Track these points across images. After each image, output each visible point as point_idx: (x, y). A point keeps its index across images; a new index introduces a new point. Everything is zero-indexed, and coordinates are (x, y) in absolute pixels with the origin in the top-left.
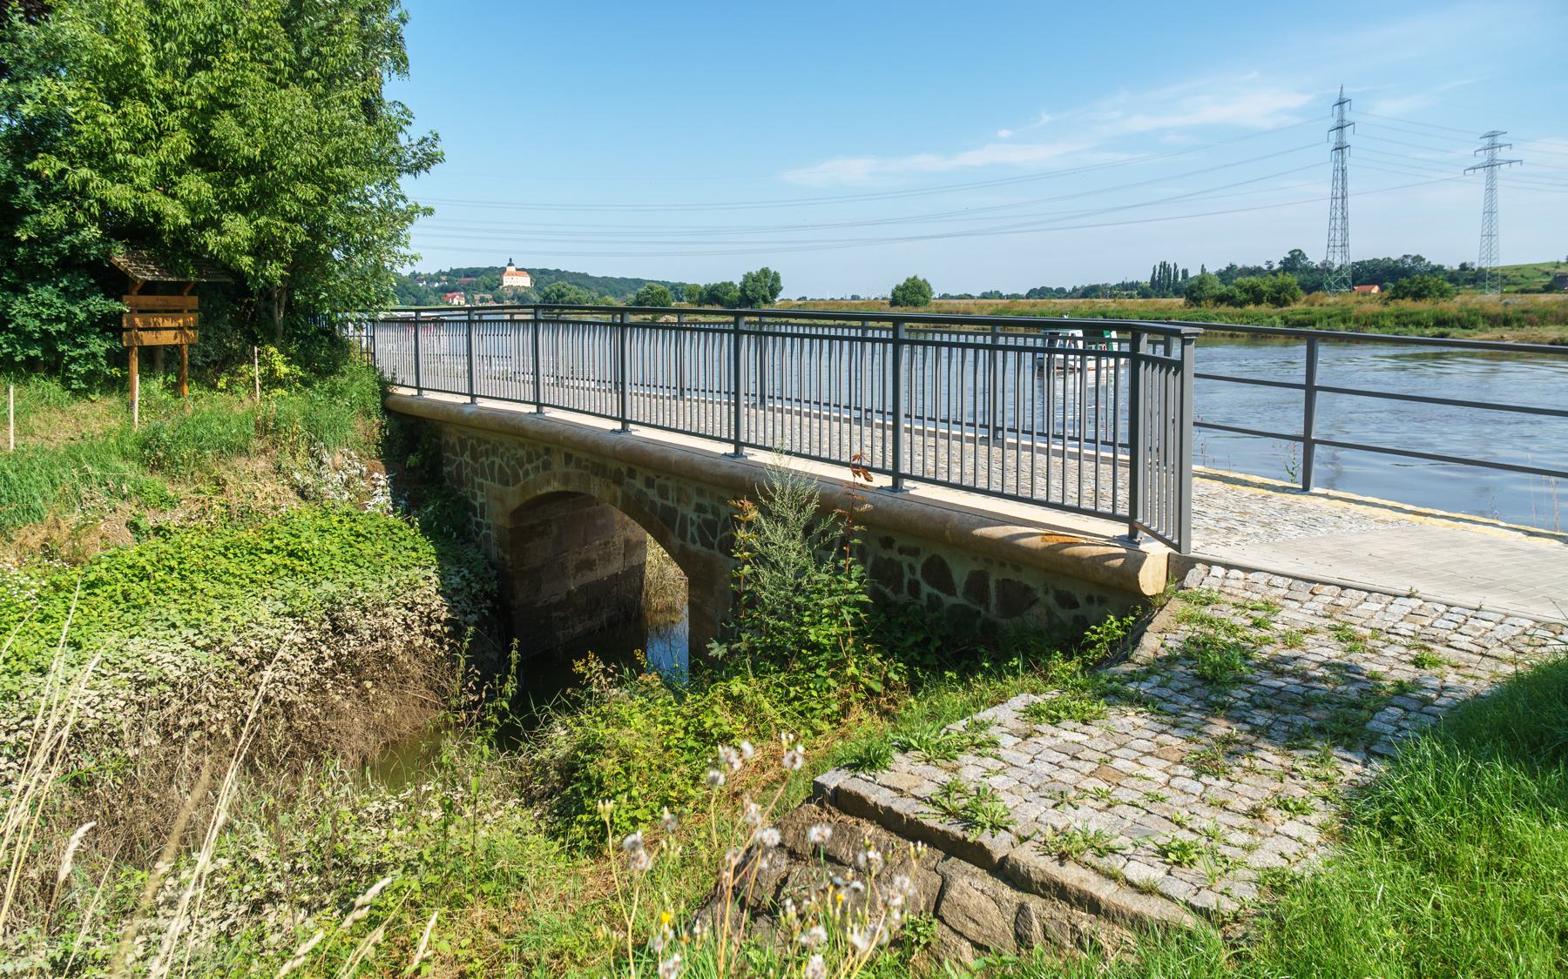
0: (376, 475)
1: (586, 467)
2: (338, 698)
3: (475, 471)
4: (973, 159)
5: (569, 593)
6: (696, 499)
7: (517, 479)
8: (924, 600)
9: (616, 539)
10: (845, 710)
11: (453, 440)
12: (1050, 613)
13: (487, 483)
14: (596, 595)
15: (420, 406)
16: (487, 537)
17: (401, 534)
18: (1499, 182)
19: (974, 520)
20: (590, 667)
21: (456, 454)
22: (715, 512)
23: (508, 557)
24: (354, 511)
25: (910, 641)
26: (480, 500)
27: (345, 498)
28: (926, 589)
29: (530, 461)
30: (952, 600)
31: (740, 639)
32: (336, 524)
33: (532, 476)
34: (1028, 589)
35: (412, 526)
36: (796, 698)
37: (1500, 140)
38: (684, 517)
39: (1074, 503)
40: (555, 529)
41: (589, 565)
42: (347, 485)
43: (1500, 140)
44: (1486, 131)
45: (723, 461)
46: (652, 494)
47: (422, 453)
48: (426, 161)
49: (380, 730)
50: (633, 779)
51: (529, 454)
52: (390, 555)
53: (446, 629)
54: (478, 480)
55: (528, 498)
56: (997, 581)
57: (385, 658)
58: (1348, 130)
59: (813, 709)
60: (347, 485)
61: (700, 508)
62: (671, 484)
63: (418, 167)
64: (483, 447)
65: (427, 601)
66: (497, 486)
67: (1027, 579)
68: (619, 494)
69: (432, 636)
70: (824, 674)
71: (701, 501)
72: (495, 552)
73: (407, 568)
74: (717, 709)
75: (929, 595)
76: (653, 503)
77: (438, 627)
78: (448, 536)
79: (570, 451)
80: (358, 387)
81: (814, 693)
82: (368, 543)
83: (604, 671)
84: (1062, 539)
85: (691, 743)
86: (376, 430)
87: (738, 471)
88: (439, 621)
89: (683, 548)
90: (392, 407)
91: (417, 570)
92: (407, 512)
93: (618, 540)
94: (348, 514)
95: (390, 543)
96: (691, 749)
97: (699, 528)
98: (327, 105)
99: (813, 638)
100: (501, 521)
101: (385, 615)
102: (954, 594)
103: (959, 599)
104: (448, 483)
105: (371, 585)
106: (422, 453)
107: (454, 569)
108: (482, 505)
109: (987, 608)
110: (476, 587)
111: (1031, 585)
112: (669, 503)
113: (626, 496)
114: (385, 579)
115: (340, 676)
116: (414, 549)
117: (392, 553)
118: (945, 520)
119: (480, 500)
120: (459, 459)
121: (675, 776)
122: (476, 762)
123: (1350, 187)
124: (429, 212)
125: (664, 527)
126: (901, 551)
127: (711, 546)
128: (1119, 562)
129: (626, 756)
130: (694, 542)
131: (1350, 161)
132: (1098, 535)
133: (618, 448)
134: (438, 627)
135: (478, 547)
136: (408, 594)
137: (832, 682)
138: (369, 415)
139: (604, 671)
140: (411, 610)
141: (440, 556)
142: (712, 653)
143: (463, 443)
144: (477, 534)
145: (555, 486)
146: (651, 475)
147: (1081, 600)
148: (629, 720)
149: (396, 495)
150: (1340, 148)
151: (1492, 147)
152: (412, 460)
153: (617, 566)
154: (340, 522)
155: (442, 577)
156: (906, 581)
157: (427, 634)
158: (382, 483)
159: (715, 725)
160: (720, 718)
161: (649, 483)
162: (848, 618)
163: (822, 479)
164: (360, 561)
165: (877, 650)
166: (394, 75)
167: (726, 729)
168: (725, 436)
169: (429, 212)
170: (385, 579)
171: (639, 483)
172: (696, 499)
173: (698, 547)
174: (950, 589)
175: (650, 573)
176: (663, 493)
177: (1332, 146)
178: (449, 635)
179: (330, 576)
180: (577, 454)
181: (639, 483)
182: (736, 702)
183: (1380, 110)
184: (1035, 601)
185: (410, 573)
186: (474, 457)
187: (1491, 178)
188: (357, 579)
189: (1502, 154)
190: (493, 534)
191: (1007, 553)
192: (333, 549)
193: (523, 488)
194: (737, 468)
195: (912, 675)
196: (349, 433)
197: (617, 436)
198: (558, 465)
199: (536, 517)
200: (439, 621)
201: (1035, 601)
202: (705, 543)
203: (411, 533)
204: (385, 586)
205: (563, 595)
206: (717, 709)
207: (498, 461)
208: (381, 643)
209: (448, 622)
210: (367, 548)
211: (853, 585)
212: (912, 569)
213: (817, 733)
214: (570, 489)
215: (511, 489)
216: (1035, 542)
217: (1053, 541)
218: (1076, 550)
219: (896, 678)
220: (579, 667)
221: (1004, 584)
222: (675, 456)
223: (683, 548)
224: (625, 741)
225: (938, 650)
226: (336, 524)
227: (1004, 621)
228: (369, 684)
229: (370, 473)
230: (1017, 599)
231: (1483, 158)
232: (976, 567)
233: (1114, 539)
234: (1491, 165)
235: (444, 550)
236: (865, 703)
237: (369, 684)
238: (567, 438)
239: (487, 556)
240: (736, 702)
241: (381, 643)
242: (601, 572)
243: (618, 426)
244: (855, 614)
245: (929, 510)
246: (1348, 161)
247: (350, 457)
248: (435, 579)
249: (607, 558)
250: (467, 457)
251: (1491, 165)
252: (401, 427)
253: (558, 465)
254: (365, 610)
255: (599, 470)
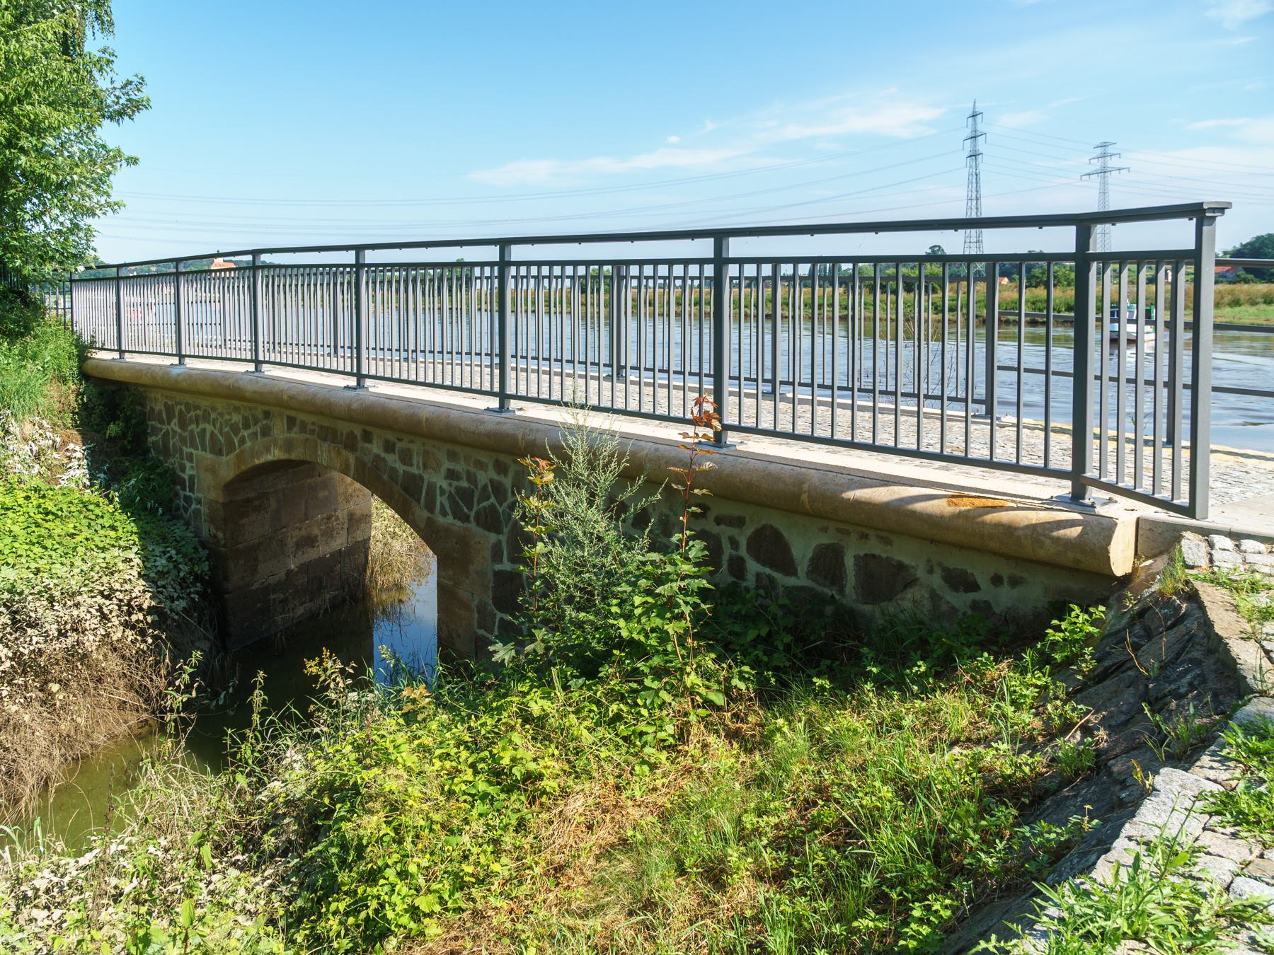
0: (71, 446)
1: (312, 432)
2: (14, 708)
3: (183, 440)
4: (647, 161)
5: (289, 573)
6: (447, 465)
7: (231, 447)
8: (750, 581)
9: (339, 513)
10: (682, 735)
11: (159, 407)
12: (934, 597)
13: (197, 453)
14: (319, 574)
15: (121, 369)
16: (197, 512)
17: (97, 511)
18: (1110, 187)
19: (842, 479)
20: (326, 667)
21: (162, 422)
22: (472, 479)
23: (220, 535)
24: (43, 486)
25: (752, 635)
26: (189, 472)
27: (35, 471)
28: (753, 567)
29: (246, 427)
30: (792, 581)
31: (533, 639)
32: (21, 501)
33: (248, 444)
34: (901, 567)
35: (111, 501)
36: (618, 717)
37: (1110, 150)
38: (431, 487)
39: (983, 453)
40: (273, 504)
41: (310, 541)
42: (37, 457)
43: (1110, 150)
44: (1098, 142)
45: (486, 417)
46: (393, 460)
47: (122, 422)
48: (129, 109)
49: (66, 741)
50: (408, 845)
51: (245, 419)
52: (84, 535)
53: (149, 619)
54: (187, 450)
55: (243, 468)
56: (857, 557)
57: (76, 656)
58: (980, 139)
59: (642, 734)
60: (37, 457)
61: (451, 475)
62: (415, 447)
63: (121, 114)
64: (193, 413)
65: (128, 587)
66: (209, 456)
67: (902, 553)
68: (352, 461)
69: (133, 628)
70: (655, 685)
71: (452, 466)
72: (206, 529)
73: (104, 549)
74: (516, 737)
75: (758, 576)
76: (394, 470)
77: (141, 616)
78: (153, 512)
79: (292, 413)
80: (55, 350)
81: (644, 712)
82: (58, 522)
83: (342, 672)
84: (978, 503)
85: (482, 786)
86: (72, 397)
87: (507, 428)
88: (140, 609)
89: (430, 522)
90: (90, 372)
91: (115, 552)
92: (107, 486)
93: (342, 514)
94: (37, 490)
95: (85, 522)
96: (484, 796)
97: (451, 497)
98: (17, 36)
99: (625, 634)
100: (213, 495)
101: (77, 605)
102: (790, 569)
103: (801, 580)
104: (153, 454)
105: (58, 569)
106: (122, 422)
107: (159, 550)
108: (191, 478)
109: (841, 591)
110: (185, 569)
111: (907, 561)
112: (414, 470)
113: (361, 465)
114: (78, 562)
115: (20, 681)
116: (113, 528)
117: (86, 533)
118: (800, 482)
119: (189, 472)
120: (165, 427)
121: (466, 838)
122: (181, 795)
123: (983, 191)
124: (133, 161)
125: (405, 497)
126: (719, 521)
127: (465, 519)
128: (1075, 532)
129: (395, 807)
130: (444, 514)
131: (984, 166)
132: (1030, 499)
133: (355, 406)
134: (141, 616)
135: (187, 524)
136: (105, 579)
137: (664, 695)
138: (65, 381)
139: (342, 672)
140: (108, 597)
141: (143, 535)
142: (496, 658)
143: (170, 410)
144: (186, 510)
145: (276, 454)
146: (391, 436)
147: (982, 580)
148: (394, 753)
149: (93, 469)
150: (974, 155)
151: (1104, 156)
152: (113, 429)
153: (340, 542)
154: (27, 498)
155: (145, 559)
156: (725, 558)
157: (126, 625)
158: (79, 455)
159: (514, 760)
160: (519, 750)
161: (389, 447)
162: (687, 610)
163: (626, 436)
164: (48, 543)
165: (710, 648)
166: (98, 34)
167: (532, 766)
168: (487, 387)
169: (133, 161)
170: (78, 562)
171: (376, 448)
172: (447, 465)
173: (450, 519)
174: (788, 566)
175: (376, 549)
176: (406, 458)
177: (967, 153)
178: (153, 625)
179: (10, 560)
180: (301, 417)
181: (376, 448)
182: (537, 725)
183: (1003, 124)
184: (911, 583)
185: (108, 555)
186: (183, 424)
187: (1104, 183)
188: (41, 563)
189: (1112, 162)
190: (204, 509)
191: (896, 522)
192: (16, 529)
193: (238, 457)
194: (503, 424)
195: (762, 682)
196: (40, 400)
197: (353, 393)
198: (279, 430)
199: (257, 488)
200: (140, 609)
201: (911, 583)
202: (459, 515)
203: (109, 511)
204: (76, 571)
205: (282, 575)
206: (516, 737)
207: (209, 428)
208: (72, 638)
209: (151, 611)
210: (58, 528)
211: (686, 568)
212: (734, 543)
213: (653, 767)
214: (293, 457)
215: (224, 459)
216: (940, 507)
217: (965, 506)
218: (1004, 517)
219: (742, 686)
220: (312, 667)
221: (865, 562)
222: (425, 413)
223: (430, 522)
224: (391, 785)
225: (788, 648)
226: (21, 501)
227: (867, 608)
228: (55, 687)
229: (64, 443)
230: (884, 579)
231: (1097, 165)
232: (825, 540)
233: (1051, 501)
234: (1103, 171)
235: (148, 528)
236: (709, 726)
237: (55, 687)
238: (292, 398)
239: (197, 534)
240: (537, 725)
241: (72, 638)
242: (324, 549)
243: (352, 382)
244: (695, 606)
245: (772, 467)
246: (981, 167)
247: (41, 426)
248: (137, 561)
249: (329, 534)
250: (174, 425)
251: (1103, 171)
252: (101, 394)
253: (279, 430)
254: (51, 600)
255: (328, 434)
